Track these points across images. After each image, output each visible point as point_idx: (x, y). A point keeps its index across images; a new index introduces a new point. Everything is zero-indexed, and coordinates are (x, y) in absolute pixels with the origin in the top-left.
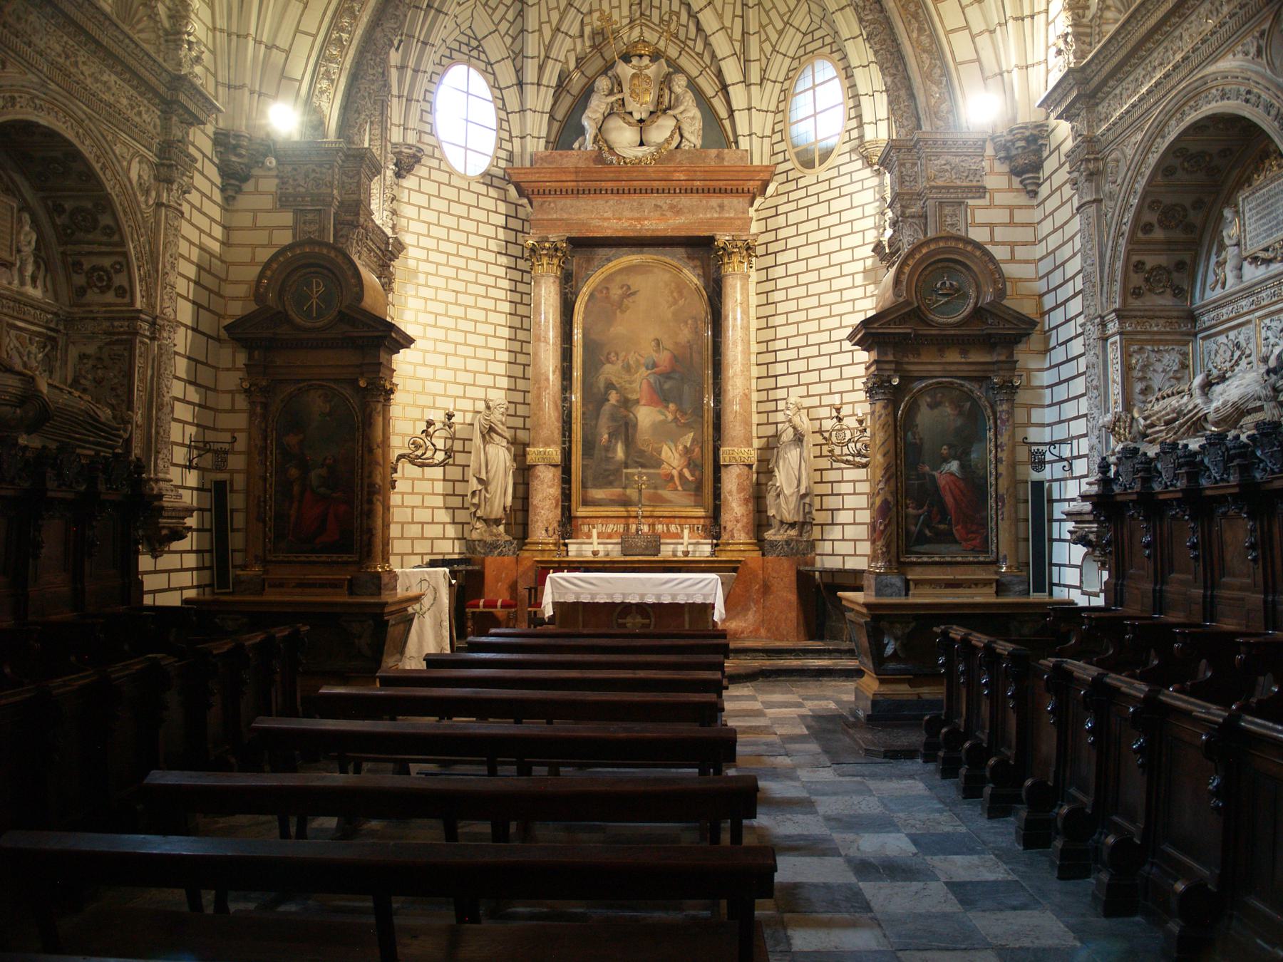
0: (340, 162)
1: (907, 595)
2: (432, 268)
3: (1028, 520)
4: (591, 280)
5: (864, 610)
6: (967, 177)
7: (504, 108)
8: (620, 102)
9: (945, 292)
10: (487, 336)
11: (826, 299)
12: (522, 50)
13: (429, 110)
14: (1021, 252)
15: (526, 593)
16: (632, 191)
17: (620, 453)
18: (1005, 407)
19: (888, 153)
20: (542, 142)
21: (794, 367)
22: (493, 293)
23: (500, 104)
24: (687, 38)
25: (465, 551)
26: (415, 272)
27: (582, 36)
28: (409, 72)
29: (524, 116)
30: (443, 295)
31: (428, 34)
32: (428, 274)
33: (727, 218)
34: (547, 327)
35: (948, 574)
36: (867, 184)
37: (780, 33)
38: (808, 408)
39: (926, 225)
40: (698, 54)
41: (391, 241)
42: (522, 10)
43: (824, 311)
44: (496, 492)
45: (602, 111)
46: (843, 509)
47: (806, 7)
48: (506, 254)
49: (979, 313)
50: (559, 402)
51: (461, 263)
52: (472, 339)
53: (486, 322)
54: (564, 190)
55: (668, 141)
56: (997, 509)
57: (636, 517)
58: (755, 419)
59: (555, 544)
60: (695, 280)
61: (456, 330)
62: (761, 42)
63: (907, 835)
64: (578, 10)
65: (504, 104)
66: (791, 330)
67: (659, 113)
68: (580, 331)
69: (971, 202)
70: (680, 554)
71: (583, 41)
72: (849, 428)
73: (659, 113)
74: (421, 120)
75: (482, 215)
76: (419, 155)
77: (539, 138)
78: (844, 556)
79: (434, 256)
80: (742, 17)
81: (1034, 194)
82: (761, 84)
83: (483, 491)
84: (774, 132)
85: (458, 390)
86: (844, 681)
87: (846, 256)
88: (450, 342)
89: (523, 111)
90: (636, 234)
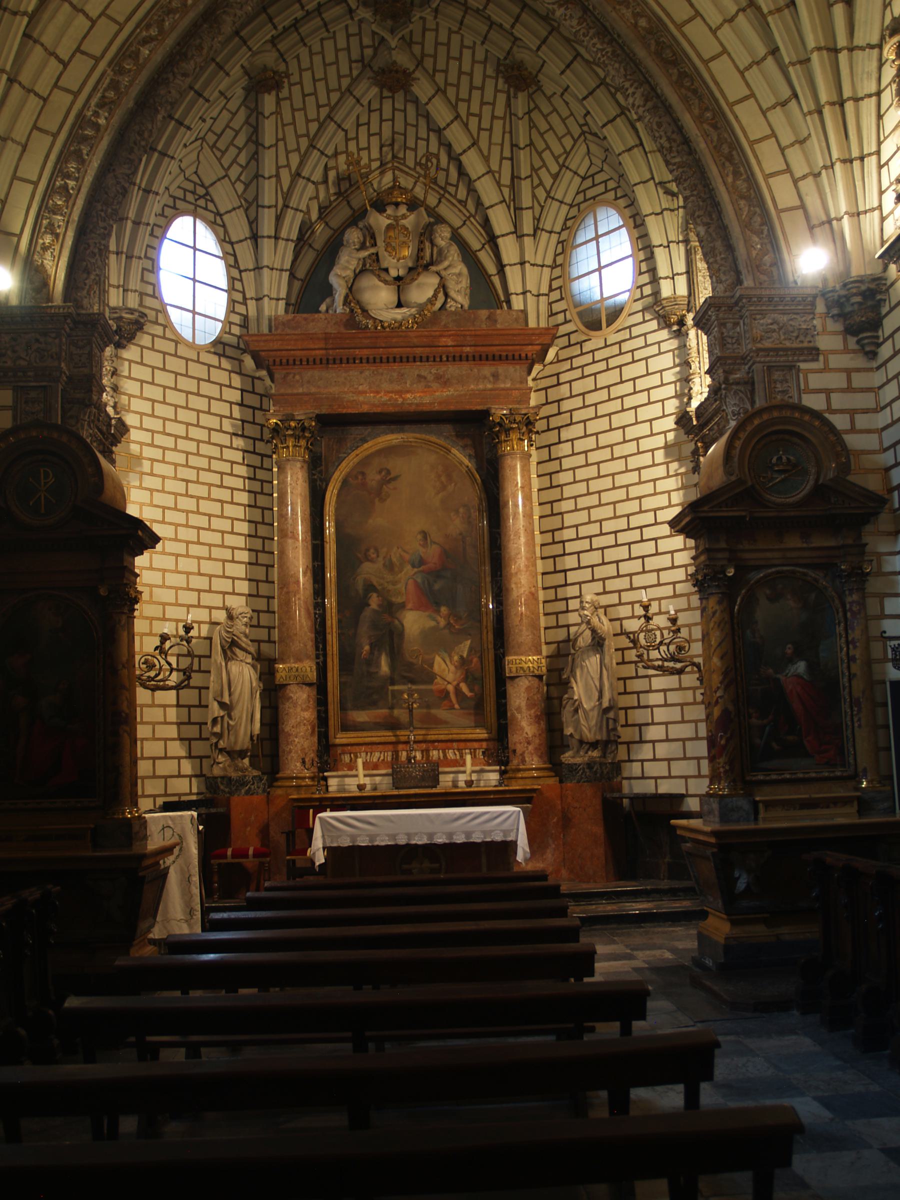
0: (68, 330)
1: (756, 819)
2: (157, 454)
3: (888, 727)
4: (344, 464)
5: (713, 840)
6: (797, 337)
7: (236, 265)
8: (374, 257)
9: (781, 468)
10: (223, 532)
11: (621, 480)
12: (256, 198)
13: (152, 267)
14: (862, 421)
15: (282, 840)
16: (391, 360)
17: (384, 667)
18: (855, 597)
19: (706, 312)
20: (282, 304)
21: (587, 559)
22: (229, 481)
23: (231, 260)
24: (447, 183)
25: (204, 790)
26: (139, 458)
27: (325, 181)
28: (129, 224)
29: (260, 275)
30: (171, 485)
31: (151, 181)
32: (153, 460)
33: (503, 389)
34: (295, 521)
35: (801, 793)
36: (665, 347)
37: (555, 177)
38: (606, 607)
39: (753, 392)
40: (460, 202)
41: (113, 422)
42: (256, 153)
43: (621, 494)
44: (241, 718)
45: (353, 267)
46: (653, 723)
47: (583, 149)
48: (243, 436)
49: (820, 491)
50: (311, 608)
51: (191, 447)
52: (206, 537)
53: (222, 516)
54: (311, 359)
55: (431, 301)
56: (852, 715)
57: (407, 743)
58: (543, 622)
59: (312, 778)
60: (466, 461)
61: (187, 526)
62: (533, 188)
63: (815, 1098)
64: (322, 153)
65: (236, 261)
66: (582, 517)
67: (420, 270)
68: (333, 524)
69: (803, 366)
70: (462, 784)
71: (327, 188)
72: (659, 629)
73: (420, 270)
74: (142, 280)
75: (214, 391)
76: (142, 321)
77: (278, 299)
78: (656, 778)
79: (160, 440)
80: (511, 159)
81: (873, 355)
82: (534, 235)
83: (226, 718)
84: (551, 290)
85: (190, 598)
86: (670, 926)
87: (644, 429)
88: (180, 541)
89: (258, 268)
90: (397, 410)
